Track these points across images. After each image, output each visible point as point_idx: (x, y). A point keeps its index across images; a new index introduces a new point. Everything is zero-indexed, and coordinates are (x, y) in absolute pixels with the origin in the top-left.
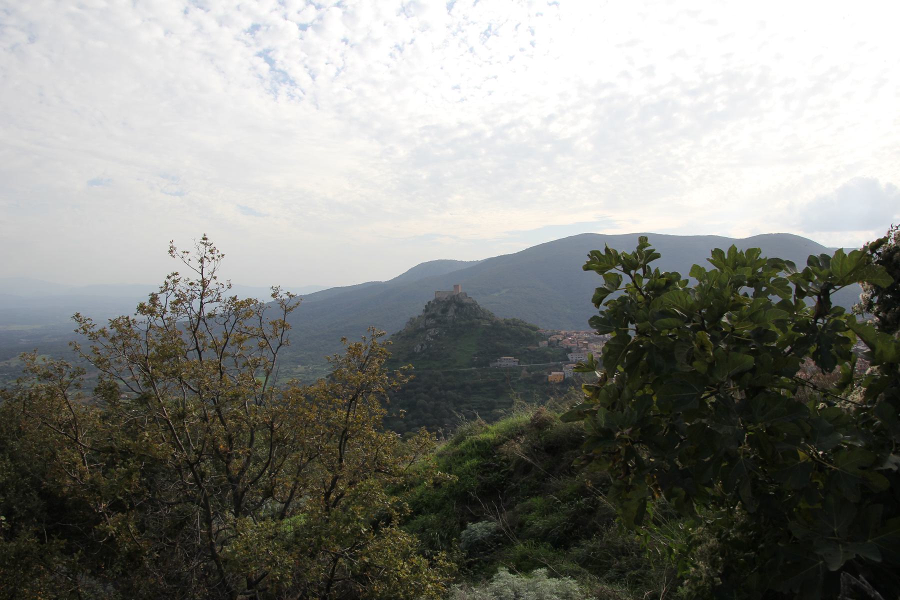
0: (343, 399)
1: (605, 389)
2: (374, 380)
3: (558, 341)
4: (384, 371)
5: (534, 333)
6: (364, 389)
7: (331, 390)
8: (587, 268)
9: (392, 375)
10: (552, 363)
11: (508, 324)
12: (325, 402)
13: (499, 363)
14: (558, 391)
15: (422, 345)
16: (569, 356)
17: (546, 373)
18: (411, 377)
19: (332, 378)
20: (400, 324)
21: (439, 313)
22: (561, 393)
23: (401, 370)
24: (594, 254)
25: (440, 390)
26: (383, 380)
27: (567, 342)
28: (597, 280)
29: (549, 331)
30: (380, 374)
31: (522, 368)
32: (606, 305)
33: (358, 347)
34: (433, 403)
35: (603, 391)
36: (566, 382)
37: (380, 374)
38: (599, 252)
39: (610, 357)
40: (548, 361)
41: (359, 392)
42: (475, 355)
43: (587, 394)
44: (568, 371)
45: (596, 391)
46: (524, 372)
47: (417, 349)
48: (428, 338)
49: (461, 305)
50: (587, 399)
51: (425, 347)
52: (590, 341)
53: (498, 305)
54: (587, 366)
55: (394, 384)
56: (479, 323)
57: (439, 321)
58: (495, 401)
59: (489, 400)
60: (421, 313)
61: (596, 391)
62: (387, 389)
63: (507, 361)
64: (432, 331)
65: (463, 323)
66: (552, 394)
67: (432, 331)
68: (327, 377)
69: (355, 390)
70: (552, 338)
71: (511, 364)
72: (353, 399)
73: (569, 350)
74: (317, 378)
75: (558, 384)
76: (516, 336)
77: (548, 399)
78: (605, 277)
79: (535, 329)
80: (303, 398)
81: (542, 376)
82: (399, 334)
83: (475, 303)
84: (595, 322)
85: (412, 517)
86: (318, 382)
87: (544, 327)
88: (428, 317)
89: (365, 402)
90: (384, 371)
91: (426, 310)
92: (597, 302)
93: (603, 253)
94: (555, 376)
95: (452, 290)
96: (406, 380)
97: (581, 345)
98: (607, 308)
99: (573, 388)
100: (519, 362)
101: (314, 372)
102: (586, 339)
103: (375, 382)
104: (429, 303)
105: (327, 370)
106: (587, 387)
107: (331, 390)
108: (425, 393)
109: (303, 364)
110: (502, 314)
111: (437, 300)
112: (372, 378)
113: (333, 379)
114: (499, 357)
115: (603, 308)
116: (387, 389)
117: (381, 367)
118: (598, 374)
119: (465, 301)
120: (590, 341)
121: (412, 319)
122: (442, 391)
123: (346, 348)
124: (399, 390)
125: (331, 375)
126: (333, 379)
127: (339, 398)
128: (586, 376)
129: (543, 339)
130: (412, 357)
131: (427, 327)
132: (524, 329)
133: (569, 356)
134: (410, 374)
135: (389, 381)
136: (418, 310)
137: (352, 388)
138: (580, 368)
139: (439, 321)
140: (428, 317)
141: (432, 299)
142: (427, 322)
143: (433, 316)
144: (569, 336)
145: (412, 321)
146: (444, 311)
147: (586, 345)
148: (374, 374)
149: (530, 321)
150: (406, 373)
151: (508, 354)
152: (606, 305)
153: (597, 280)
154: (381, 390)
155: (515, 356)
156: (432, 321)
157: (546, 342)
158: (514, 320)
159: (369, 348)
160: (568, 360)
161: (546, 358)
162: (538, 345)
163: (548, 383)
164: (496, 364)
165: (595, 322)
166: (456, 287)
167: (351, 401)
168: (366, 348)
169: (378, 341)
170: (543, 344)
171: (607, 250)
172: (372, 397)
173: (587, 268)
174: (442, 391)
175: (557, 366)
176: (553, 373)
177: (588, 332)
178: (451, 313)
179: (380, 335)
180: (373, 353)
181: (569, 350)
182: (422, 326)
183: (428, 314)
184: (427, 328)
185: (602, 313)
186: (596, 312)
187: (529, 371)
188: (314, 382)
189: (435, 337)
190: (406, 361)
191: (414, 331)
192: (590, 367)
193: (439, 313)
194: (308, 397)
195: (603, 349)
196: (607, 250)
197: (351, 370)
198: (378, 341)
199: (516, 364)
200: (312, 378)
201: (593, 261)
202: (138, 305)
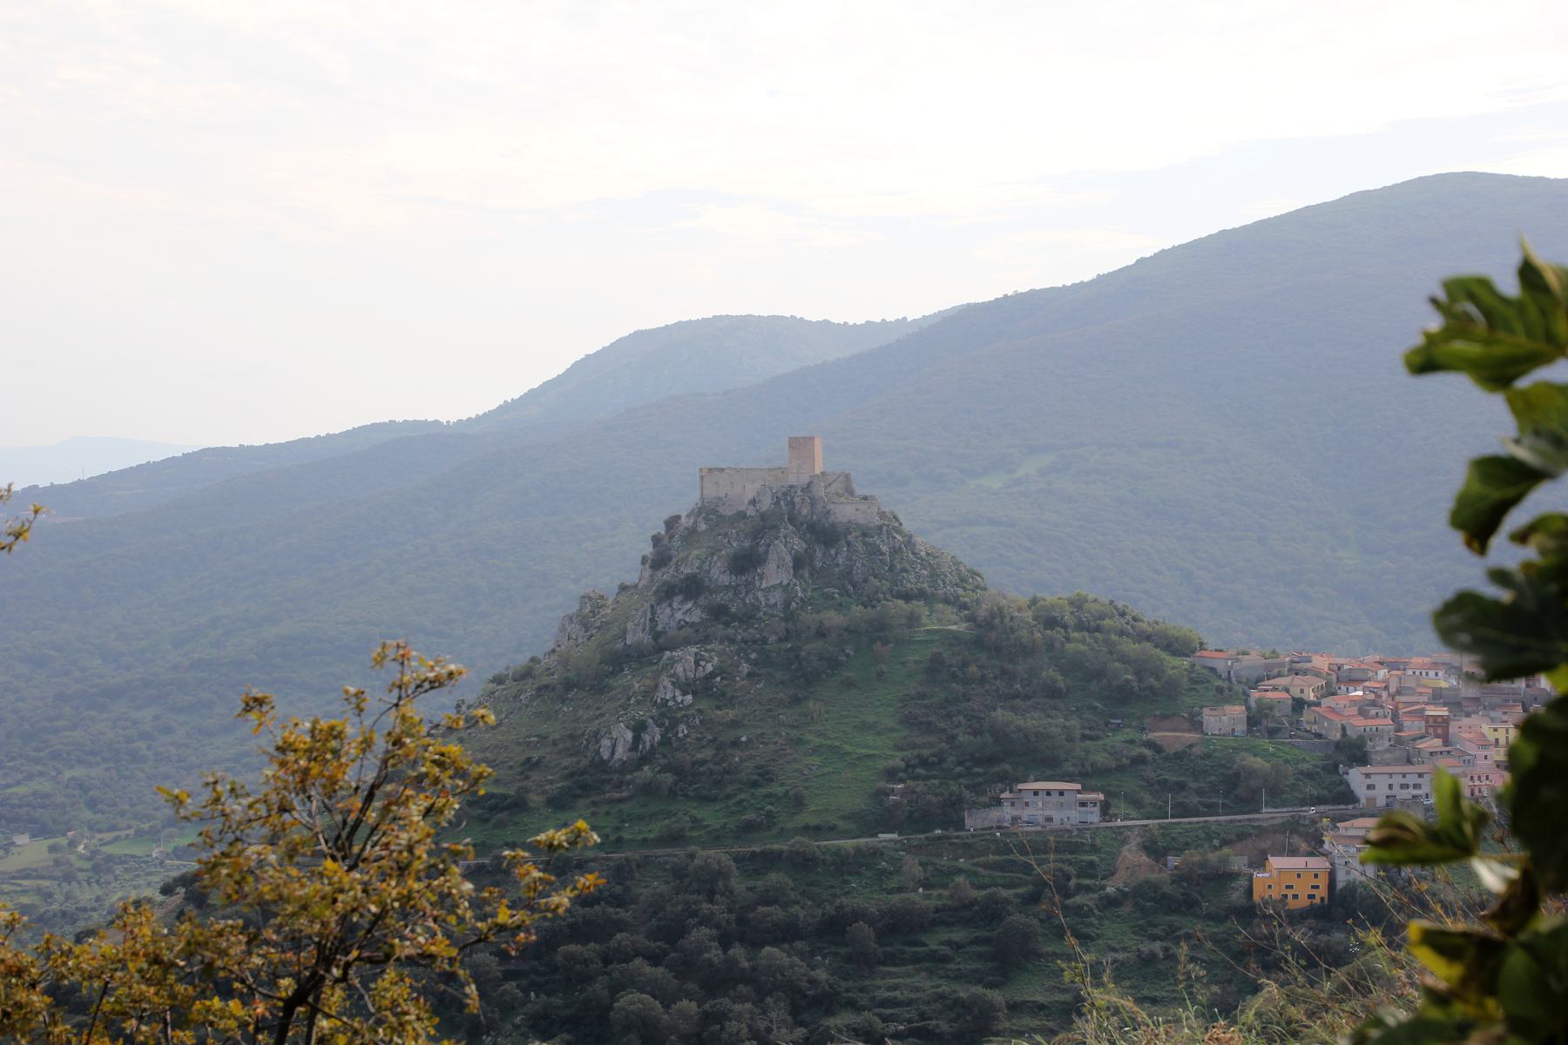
0: (246, 1000)
1: (1528, 948)
2: (406, 899)
3: (1299, 705)
4: (456, 855)
5: (1176, 665)
6: (355, 945)
7: (188, 955)
8: (1426, 362)
9: (492, 874)
10: (1270, 815)
11: (1051, 622)
12: (156, 1017)
13: (1007, 812)
14: (1299, 951)
15: (639, 728)
16: (1356, 777)
17: (1239, 863)
18: (587, 881)
19: (193, 892)
20: (529, 630)
21: (719, 574)
22: (1320, 960)
23: (534, 848)
24: (1466, 301)
25: (725, 941)
26: (445, 900)
27: (1344, 713)
28: (1482, 421)
29: (1253, 660)
30: (432, 872)
31: (1120, 836)
32: (1521, 537)
33: (326, 742)
34: (688, 1006)
35: (1516, 962)
36: (1340, 907)
37: (432, 872)
38: (1484, 283)
39: (1548, 794)
40: (1250, 803)
41: (326, 960)
42: (891, 774)
43: (1439, 972)
44: (1348, 853)
45: (1478, 957)
46: (1132, 856)
47: (617, 743)
48: (667, 691)
49: (824, 534)
50: (1438, 998)
51: (653, 735)
52: (1457, 705)
53: (1006, 533)
54: (1434, 836)
55: (504, 916)
56: (913, 620)
57: (718, 613)
58: (996, 997)
59: (964, 992)
60: (633, 574)
61: (1478, 957)
62: (468, 945)
63: (1047, 806)
64: (684, 661)
65: (833, 618)
66: (1272, 966)
67: (684, 661)
68: (167, 890)
69: (308, 955)
70: (1273, 694)
71: (1073, 816)
72: (298, 998)
73: (1356, 752)
74: (115, 898)
75: (1296, 918)
76: (1097, 682)
77: (1256, 989)
78: (1524, 407)
79: (1178, 646)
80: (38, 1000)
81: (1223, 878)
82: (525, 674)
83: (889, 525)
84: (1464, 619)
86: (118, 919)
87: (1228, 636)
88: (667, 593)
89: (356, 1006)
90: (456, 855)
91: (659, 560)
92: (1478, 524)
93: (1509, 285)
94: (1287, 876)
96: (562, 900)
97: (1412, 727)
98: (1530, 552)
99: (1374, 937)
100: (1105, 808)
101: (101, 867)
102: (1437, 696)
103: (408, 909)
104: (672, 522)
105: (171, 854)
106: (1438, 942)
107: (188, 955)
108: (655, 959)
109: (40, 831)
111: (707, 510)
112: (392, 889)
113: (199, 899)
114: (1009, 780)
115: (1505, 552)
116: (468, 945)
117: (438, 836)
118: (1492, 875)
119: (845, 512)
120: (1457, 705)
121: (593, 603)
122: (738, 951)
123: (268, 743)
124: (525, 950)
125: (186, 881)
126: (199, 899)
127: (227, 993)
128: (1438, 880)
129: (1223, 696)
130: (587, 784)
131: (661, 643)
132: (1130, 647)
133: (1356, 777)
134: (582, 866)
135: (477, 904)
136: (614, 559)
137: (296, 942)
138: (1395, 844)
139: (718, 613)
140: (667, 593)
141: (684, 504)
142: (664, 613)
143: (692, 588)
144: (1354, 681)
145: (589, 614)
146: (746, 563)
147: (1439, 727)
148: (402, 870)
149: (1097, 593)
150: (560, 865)
151: (1050, 766)
152: (1521, 537)
153: (1482, 421)
154: (441, 948)
155: (1088, 775)
156: (684, 612)
157: (1237, 711)
158: (1078, 603)
159: (381, 744)
160: (1348, 797)
161: (1235, 789)
162: (1196, 725)
163: (1248, 912)
164: (994, 814)
165: (1464, 619)
166: (801, 446)
167: (290, 1004)
168: (367, 744)
169: (421, 709)
170: (1224, 720)
171: (1529, 273)
172: (392, 986)
173: (1426, 362)
174: (738, 951)
175: (1293, 826)
176: (1276, 862)
177: (1439, 669)
178: (775, 573)
179: (436, 683)
180: (397, 770)
181: (1356, 752)
182: (637, 636)
183: (665, 575)
184: (661, 643)
185: (1500, 577)
186: (1468, 573)
187: (1155, 850)
188: (96, 918)
189: (701, 688)
190: (560, 804)
191: (599, 664)
192: (1452, 841)
193: (719, 574)
194: (63, 997)
195: (1512, 753)
196: (1529, 273)
197: (292, 852)
198: (421, 709)
199: (1094, 816)
200: (86, 896)
201: (1457, 326)
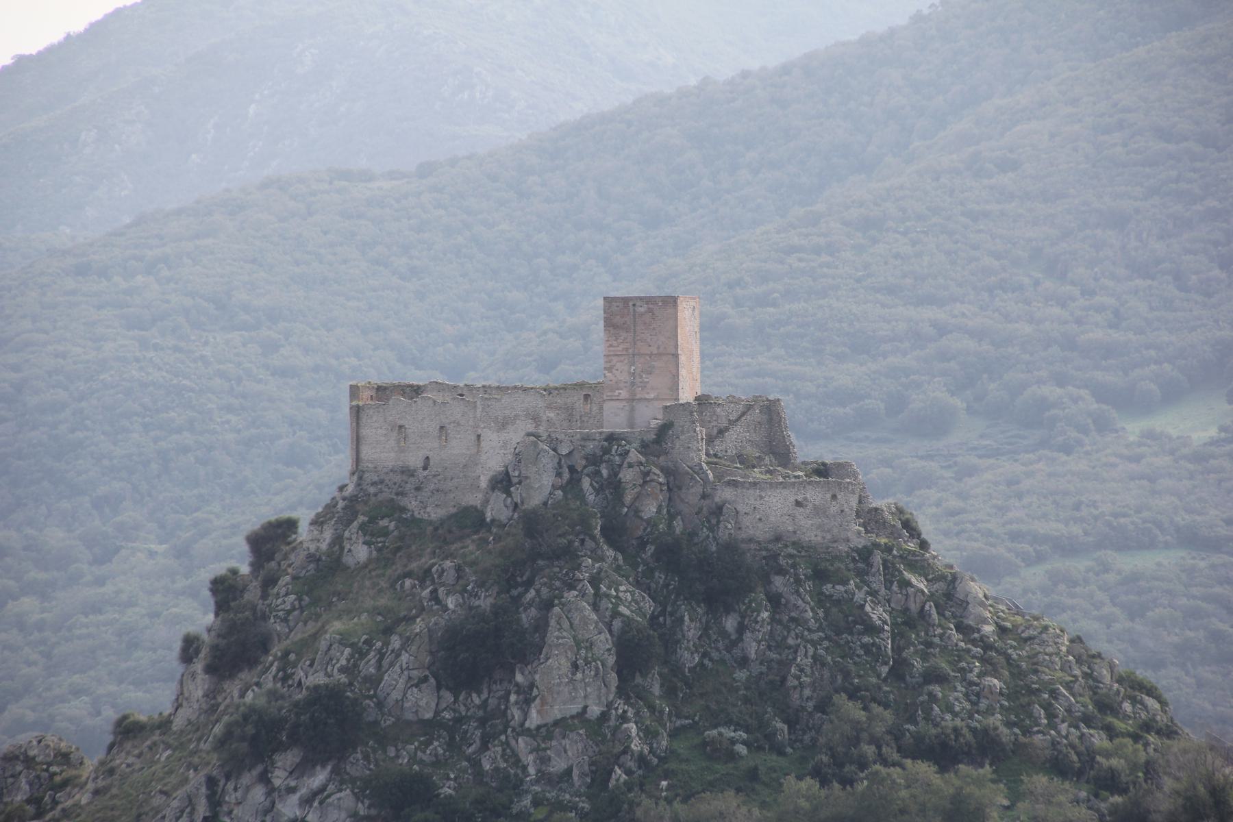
21: (407, 690)
49: (706, 572)
83: (893, 545)
85: (899, 233)
88: (254, 744)
91: (233, 645)
95: (586, 355)
104: (270, 540)
110: (1013, 650)
111: (371, 506)
119: (767, 510)
140: (254, 744)
141: (305, 484)
143: (327, 727)
146: (483, 655)
166: (637, 320)
178: (567, 683)
183: (250, 692)
193: (407, 690)
202: (178, 645)
